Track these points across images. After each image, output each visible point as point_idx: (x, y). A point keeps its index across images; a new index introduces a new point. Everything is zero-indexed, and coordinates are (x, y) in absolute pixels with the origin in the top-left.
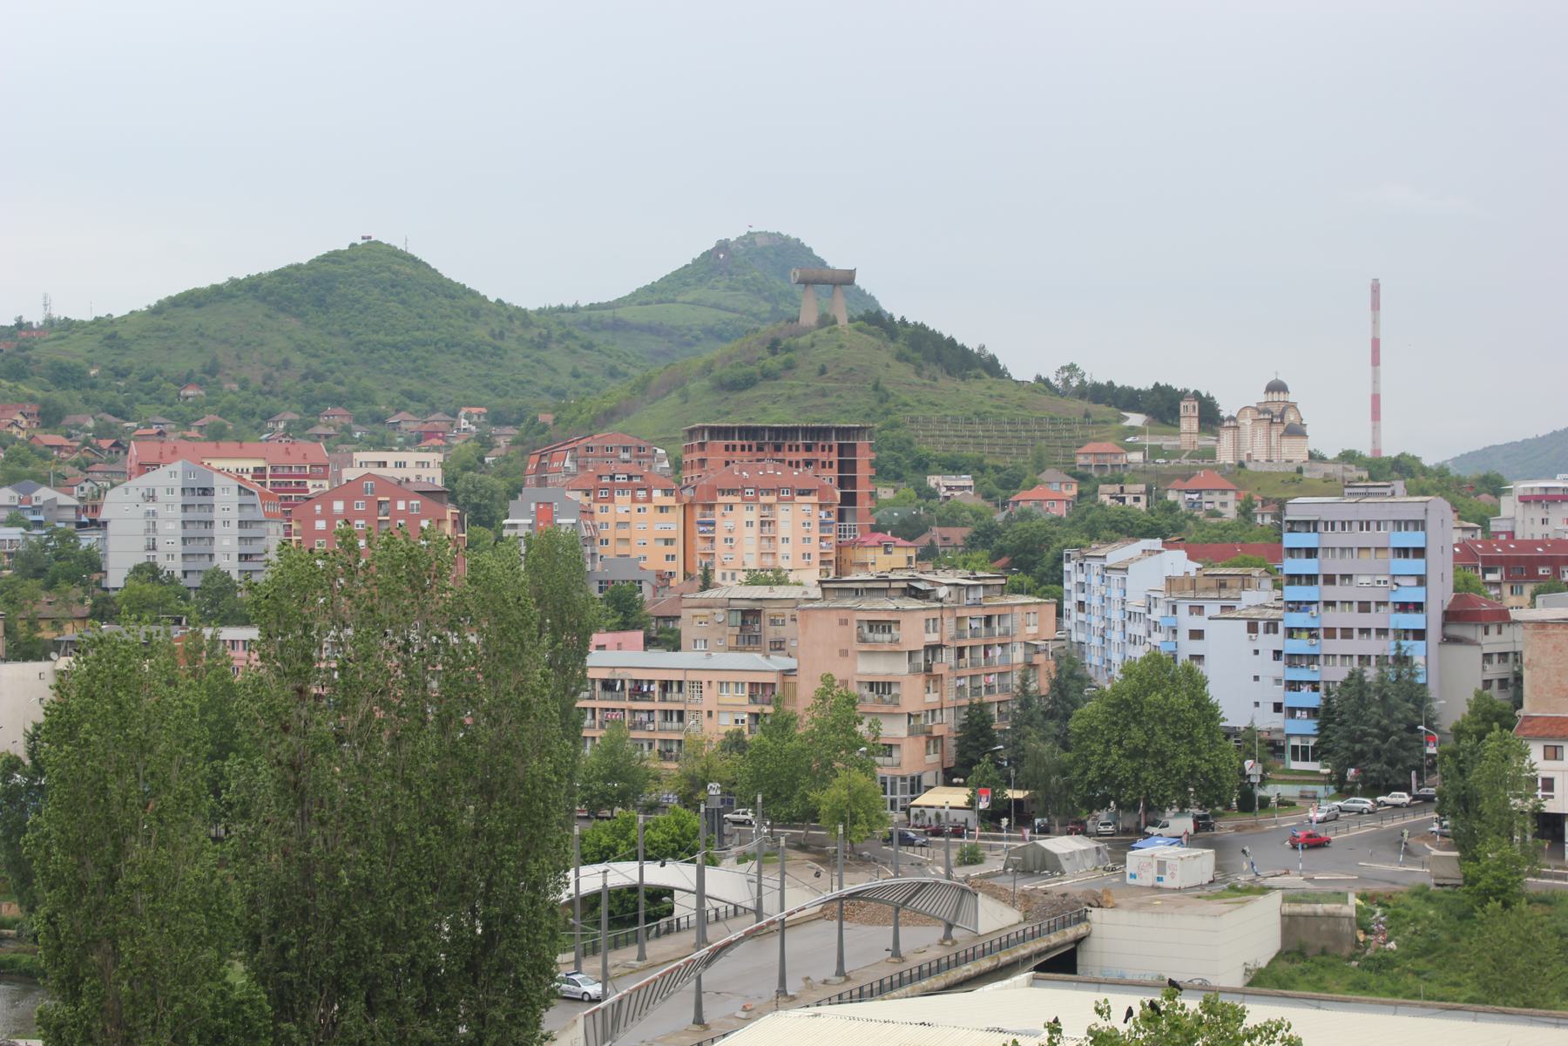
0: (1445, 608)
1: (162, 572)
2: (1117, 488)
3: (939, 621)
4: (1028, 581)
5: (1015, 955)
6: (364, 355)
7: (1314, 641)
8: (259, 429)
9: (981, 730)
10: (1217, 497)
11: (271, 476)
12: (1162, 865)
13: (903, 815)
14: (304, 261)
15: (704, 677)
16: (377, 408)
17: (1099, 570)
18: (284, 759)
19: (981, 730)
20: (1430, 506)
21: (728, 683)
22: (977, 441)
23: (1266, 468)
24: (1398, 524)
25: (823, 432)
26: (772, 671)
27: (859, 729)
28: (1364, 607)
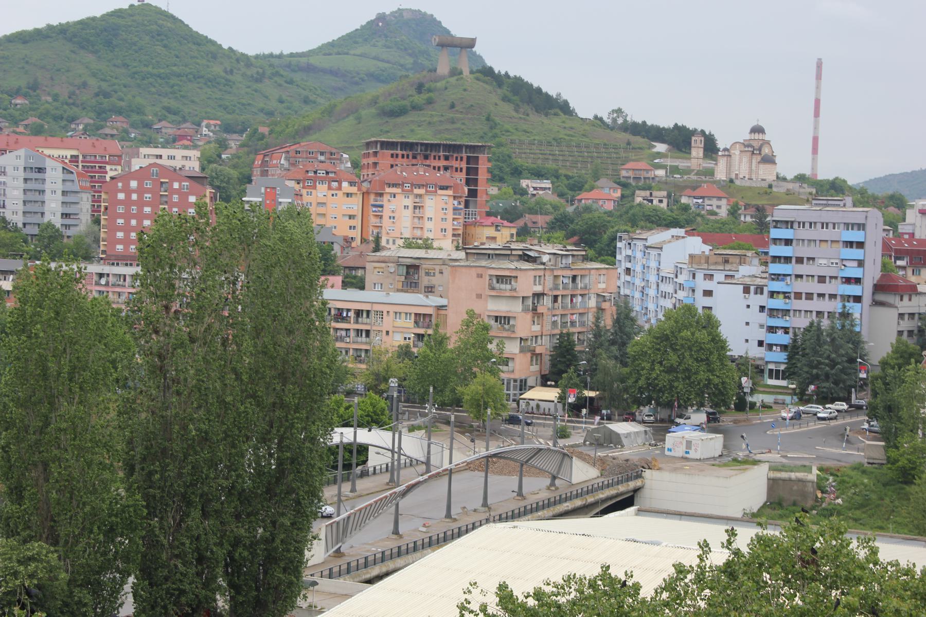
0: (875, 282)
1: (9, 223)
2: (648, 193)
3: (543, 277)
4: (591, 253)
5: (597, 498)
6: (138, 81)
7: (787, 301)
8: (66, 128)
9: (567, 351)
10: (715, 202)
11: (82, 162)
12: (689, 444)
13: (514, 405)
14: (98, 15)
15: (385, 308)
16: (146, 118)
17: (642, 248)
18: (155, 350)
19: (567, 351)
20: (869, 215)
21: (400, 313)
22: (555, 158)
23: (747, 184)
24: (847, 226)
25: (457, 148)
26: (431, 306)
27: (490, 346)
28: (822, 279)
